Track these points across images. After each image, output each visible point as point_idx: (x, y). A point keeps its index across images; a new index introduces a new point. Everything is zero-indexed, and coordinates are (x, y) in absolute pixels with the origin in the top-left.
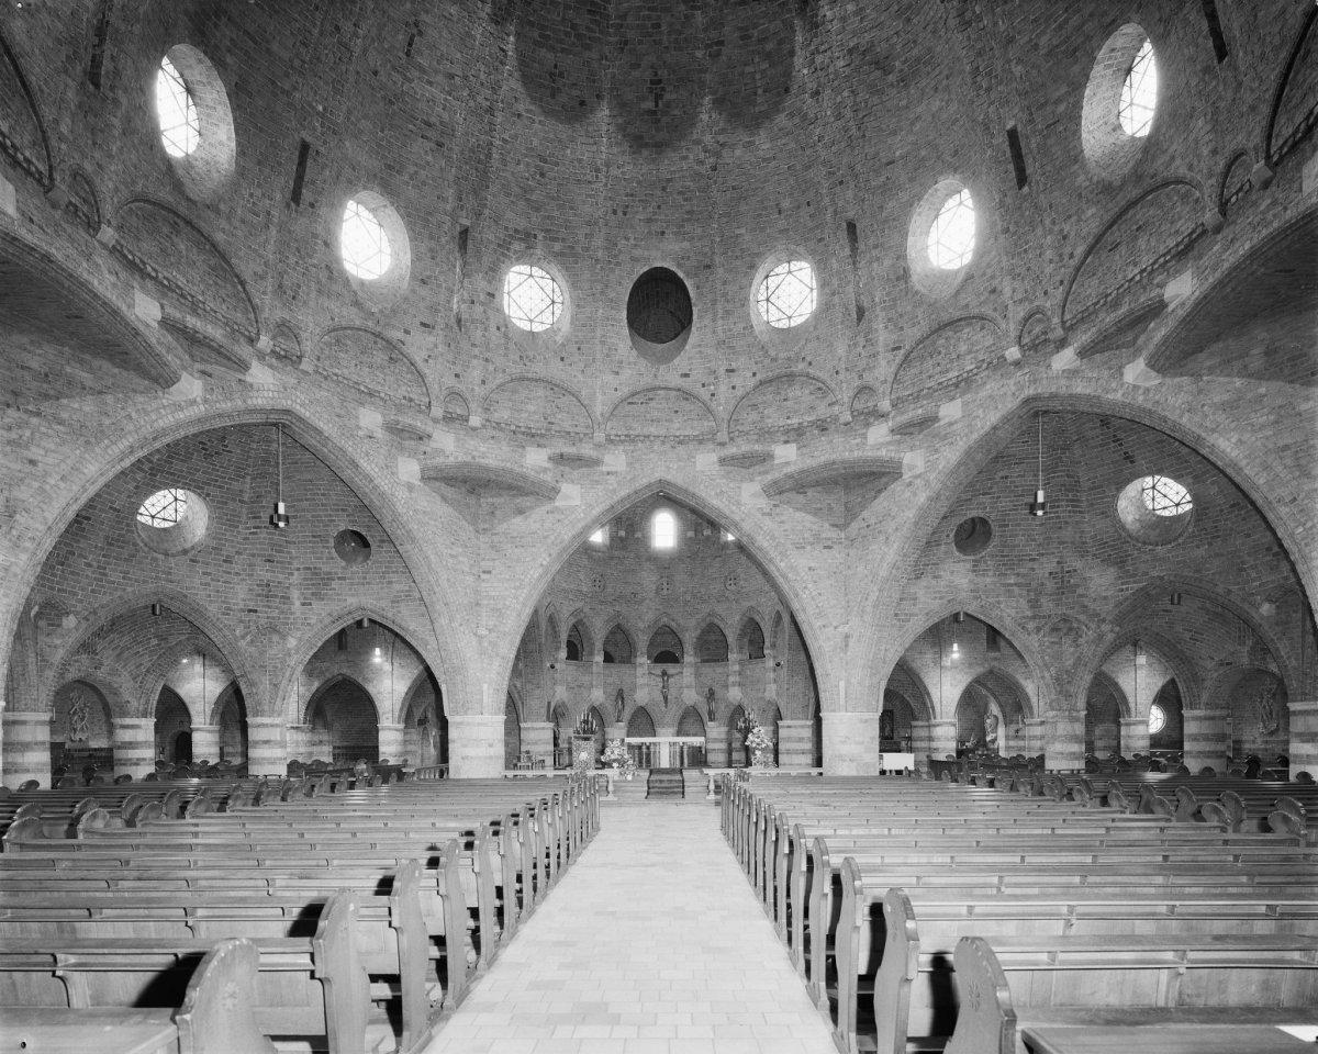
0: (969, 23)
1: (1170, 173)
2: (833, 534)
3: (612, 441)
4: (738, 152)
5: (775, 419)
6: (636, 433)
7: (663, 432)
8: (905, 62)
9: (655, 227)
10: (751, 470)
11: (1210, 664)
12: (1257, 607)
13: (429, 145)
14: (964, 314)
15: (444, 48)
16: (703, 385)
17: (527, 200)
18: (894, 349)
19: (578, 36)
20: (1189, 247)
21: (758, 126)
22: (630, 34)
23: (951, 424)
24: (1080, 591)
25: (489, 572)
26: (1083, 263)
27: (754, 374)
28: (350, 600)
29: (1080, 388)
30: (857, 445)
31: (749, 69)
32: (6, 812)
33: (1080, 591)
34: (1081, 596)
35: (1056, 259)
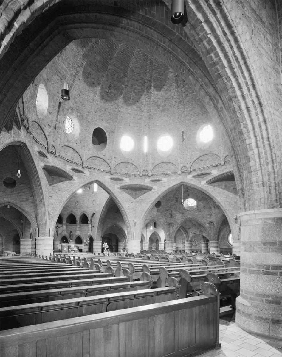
0: (179, 109)
1: (214, 153)
2: (133, 199)
3: (86, 168)
4: (124, 109)
5: (124, 171)
6: (92, 167)
7: (98, 168)
8: (162, 108)
10: (117, 182)
11: (191, 233)
12: (206, 224)
13: (58, 78)
14: (169, 161)
15: (69, 56)
16: (108, 159)
17: (75, 100)
19: (98, 68)
20: (217, 166)
21: (129, 106)
22: (109, 74)
23: (164, 182)
24: (175, 218)
25: (52, 197)
26: (195, 161)
28: (5, 199)
29: (192, 183)
31: (130, 93)
33: (175, 218)
35: (190, 158)
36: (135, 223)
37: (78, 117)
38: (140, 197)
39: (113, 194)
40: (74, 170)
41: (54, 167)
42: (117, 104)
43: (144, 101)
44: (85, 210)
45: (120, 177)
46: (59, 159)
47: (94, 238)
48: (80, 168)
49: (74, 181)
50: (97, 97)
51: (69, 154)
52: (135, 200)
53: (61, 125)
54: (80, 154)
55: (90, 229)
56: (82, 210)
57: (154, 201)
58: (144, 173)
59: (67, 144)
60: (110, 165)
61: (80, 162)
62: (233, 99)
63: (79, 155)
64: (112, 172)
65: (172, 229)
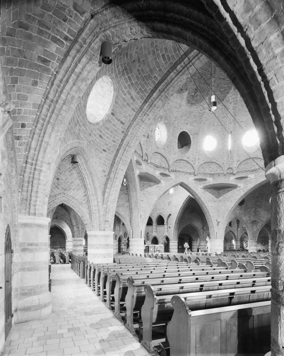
2: (216, 199)
3: (172, 171)
7: (183, 171)
9: (186, 122)
10: (200, 182)
14: (257, 157)
18: (238, 161)
25: (143, 201)
27: (203, 161)
30: (227, 180)
32: (166, 264)
34: (259, 216)
36: (219, 222)
37: (166, 124)
38: (223, 196)
39: (197, 195)
40: (162, 174)
41: (147, 173)
42: (202, 106)
43: (230, 98)
44: (160, 212)
45: (204, 178)
46: (150, 165)
47: (170, 239)
48: (167, 172)
49: (162, 185)
50: (184, 102)
51: (157, 160)
52: (217, 199)
53: (152, 133)
54: (167, 159)
55: (167, 230)
56: (157, 211)
57: (240, 199)
58: (228, 172)
59: (156, 150)
60: (194, 166)
61: (167, 167)
62: (49, 72)
63: (166, 159)
64: (196, 173)
65: (256, 227)
